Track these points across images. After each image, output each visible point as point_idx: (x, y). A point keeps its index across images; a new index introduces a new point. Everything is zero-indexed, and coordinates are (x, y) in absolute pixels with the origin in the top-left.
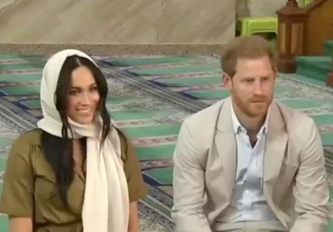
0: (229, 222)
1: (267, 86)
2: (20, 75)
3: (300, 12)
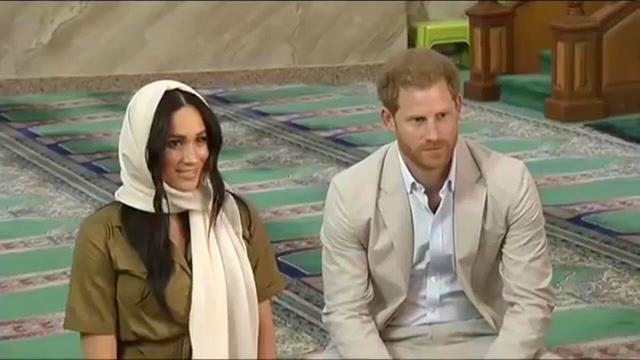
0: (408, 325)
1: (447, 125)
2: (91, 122)
3: (504, 10)
